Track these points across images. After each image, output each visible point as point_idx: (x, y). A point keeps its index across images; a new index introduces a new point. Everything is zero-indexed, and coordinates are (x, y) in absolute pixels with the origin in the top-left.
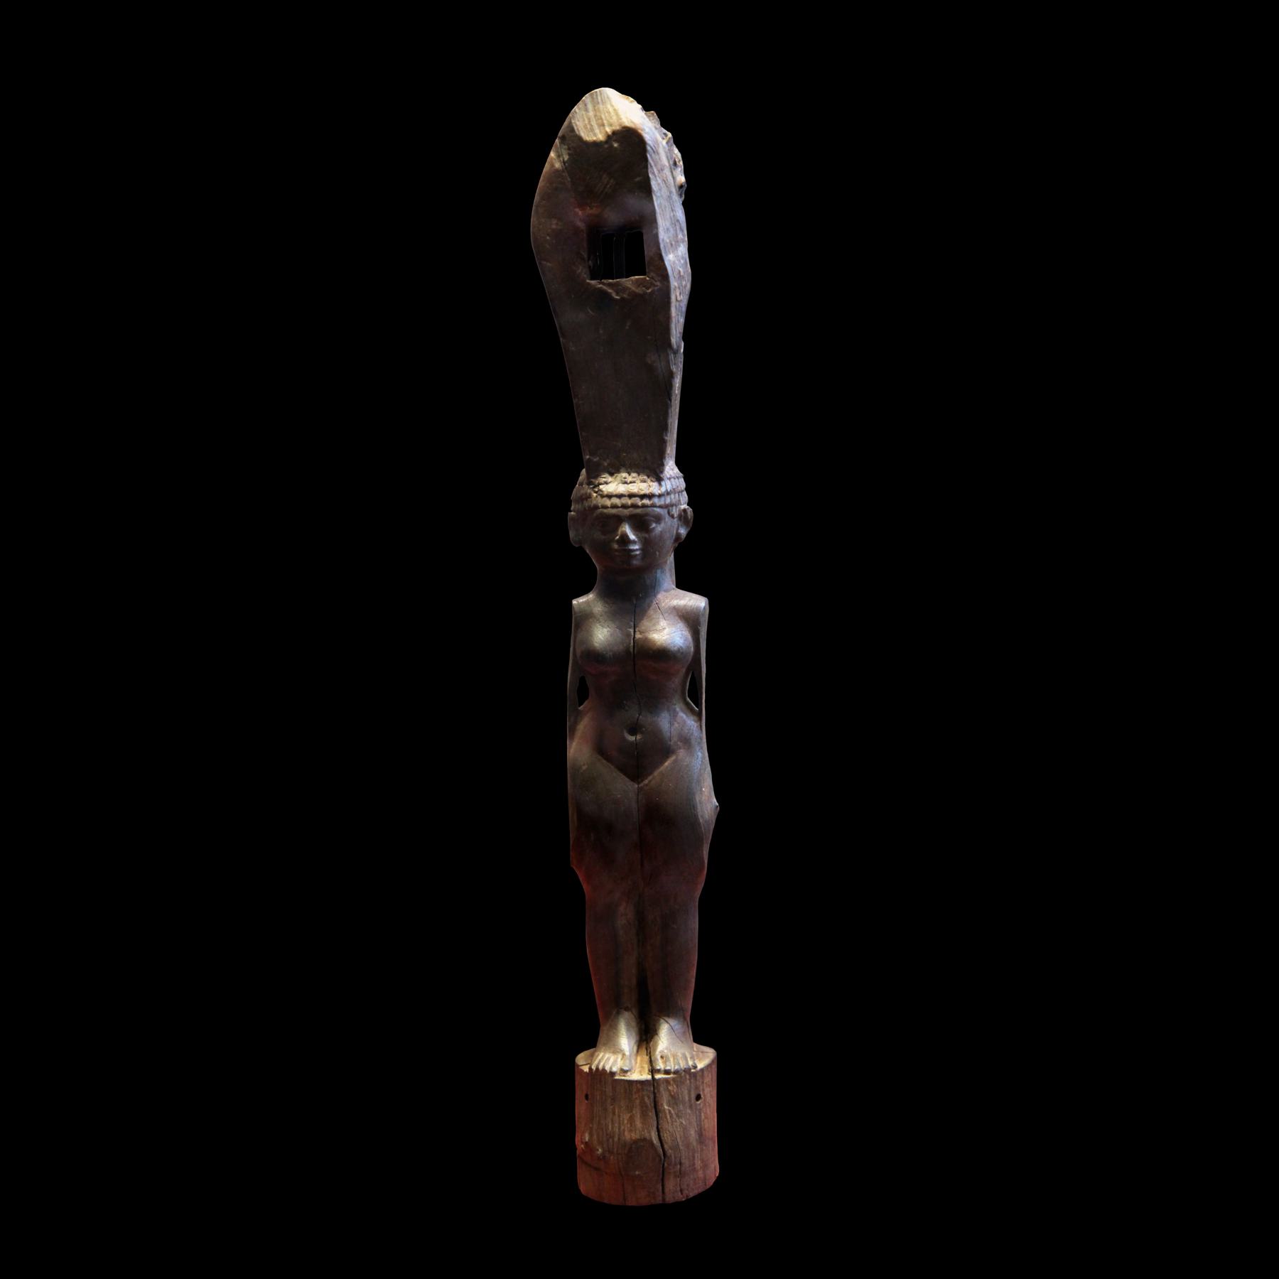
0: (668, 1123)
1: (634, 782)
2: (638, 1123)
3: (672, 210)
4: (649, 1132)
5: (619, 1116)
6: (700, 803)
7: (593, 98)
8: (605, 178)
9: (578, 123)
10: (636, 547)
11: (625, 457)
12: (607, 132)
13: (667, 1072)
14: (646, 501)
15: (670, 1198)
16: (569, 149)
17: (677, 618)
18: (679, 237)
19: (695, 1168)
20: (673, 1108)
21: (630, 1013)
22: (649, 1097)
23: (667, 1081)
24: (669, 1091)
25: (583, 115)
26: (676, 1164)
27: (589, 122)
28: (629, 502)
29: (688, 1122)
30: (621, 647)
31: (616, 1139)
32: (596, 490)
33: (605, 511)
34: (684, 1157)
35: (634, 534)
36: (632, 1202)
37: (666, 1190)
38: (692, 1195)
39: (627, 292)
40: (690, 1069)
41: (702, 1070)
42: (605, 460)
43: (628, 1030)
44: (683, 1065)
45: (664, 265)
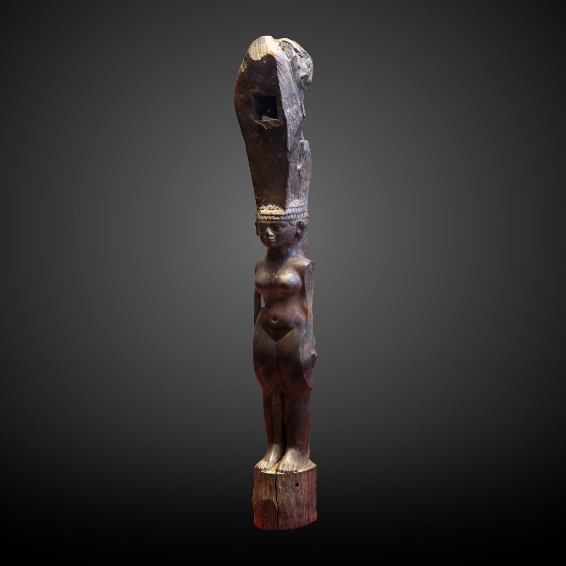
0: (280, 494)
1: (275, 341)
2: (268, 492)
3: (290, 90)
4: (272, 497)
5: (262, 489)
6: (302, 353)
7: (258, 41)
8: (261, 76)
9: (251, 52)
10: (273, 238)
11: (271, 198)
12: (261, 56)
13: (282, 471)
14: (277, 218)
16: (247, 64)
17: (294, 270)
18: (294, 101)
19: (293, 516)
20: (283, 488)
21: (278, 444)
22: (273, 482)
23: (281, 475)
24: (282, 480)
25: (254, 48)
26: (283, 513)
27: (256, 52)
28: (270, 218)
29: (290, 495)
30: (269, 282)
31: (260, 499)
33: (261, 221)
34: (287, 511)
35: (272, 232)
37: (279, 524)
38: (291, 528)
39: (270, 126)
40: (293, 472)
41: (301, 473)
42: (263, 199)
43: (275, 452)
44: (290, 469)
45: (284, 114)
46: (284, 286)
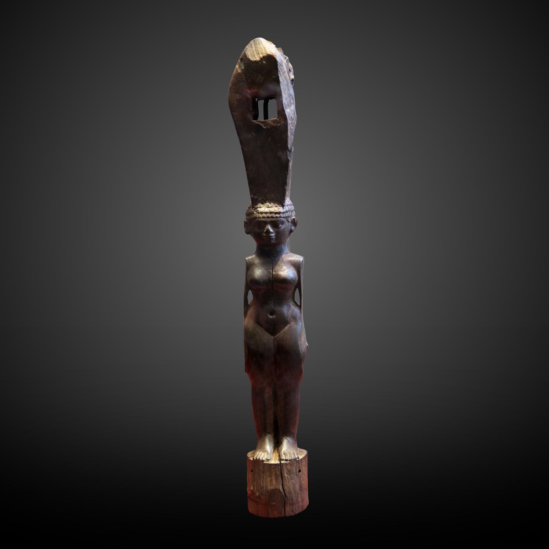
0: (287, 482)
2: (274, 482)
3: (289, 90)
4: (279, 486)
5: (266, 479)
6: (301, 345)
8: (260, 76)
9: (248, 53)
10: (273, 235)
11: (268, 196)
12: (260, 57)
13: (286, 460)
14: (277, 215)
15: (287, 514)
16: (244, 64)
17: (291, 265)
18: (292, 102)
19: (298, 501)
20: (289, 476)
21: (270, 435)
22: (279, 471)
23: (286, 464)
24: (287, 468)
25: (250, 49)
26: (290, 500)
27: (253, 52)
28: (270, 215)
29: (295, 481)
30: (267, 278)
31: (264, 489)
32: (256, 210)
33: (260, 219)
34: (293, 497)
35: (272, 229)
36: (271, 516)
37: (286, 511)
38: (297, 513)
39: (269, 125)
40: (296, 459)
41: (301, 459)
42: (260, 197)
43: (270, 442)
44: (293, 457)
45: (285, 114)
46: (284, 281)
